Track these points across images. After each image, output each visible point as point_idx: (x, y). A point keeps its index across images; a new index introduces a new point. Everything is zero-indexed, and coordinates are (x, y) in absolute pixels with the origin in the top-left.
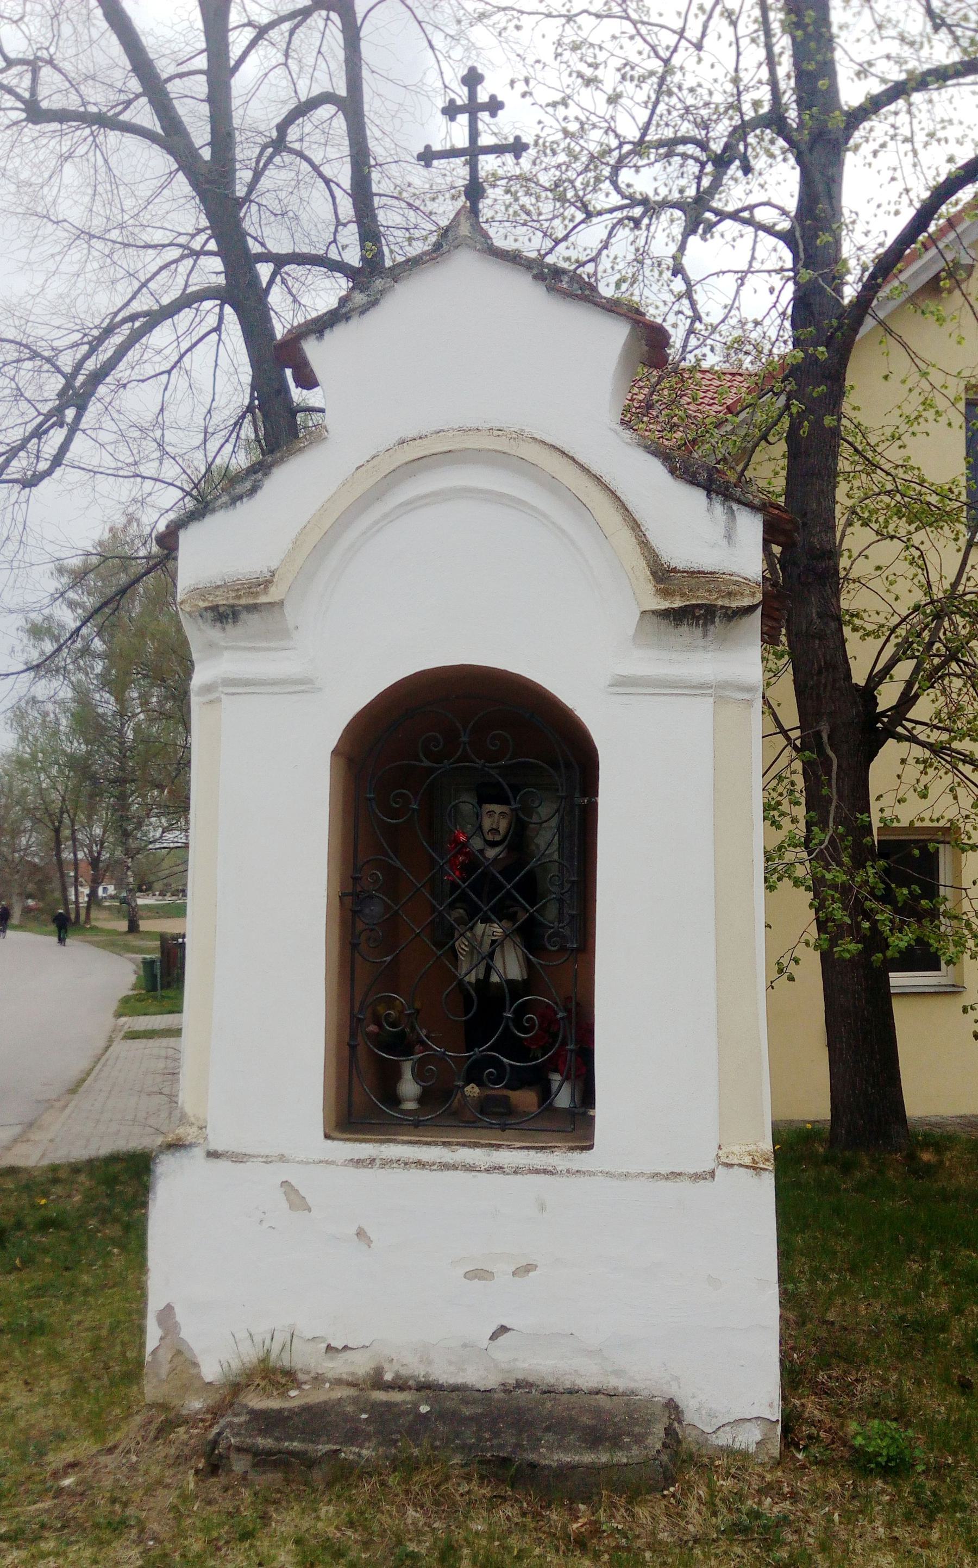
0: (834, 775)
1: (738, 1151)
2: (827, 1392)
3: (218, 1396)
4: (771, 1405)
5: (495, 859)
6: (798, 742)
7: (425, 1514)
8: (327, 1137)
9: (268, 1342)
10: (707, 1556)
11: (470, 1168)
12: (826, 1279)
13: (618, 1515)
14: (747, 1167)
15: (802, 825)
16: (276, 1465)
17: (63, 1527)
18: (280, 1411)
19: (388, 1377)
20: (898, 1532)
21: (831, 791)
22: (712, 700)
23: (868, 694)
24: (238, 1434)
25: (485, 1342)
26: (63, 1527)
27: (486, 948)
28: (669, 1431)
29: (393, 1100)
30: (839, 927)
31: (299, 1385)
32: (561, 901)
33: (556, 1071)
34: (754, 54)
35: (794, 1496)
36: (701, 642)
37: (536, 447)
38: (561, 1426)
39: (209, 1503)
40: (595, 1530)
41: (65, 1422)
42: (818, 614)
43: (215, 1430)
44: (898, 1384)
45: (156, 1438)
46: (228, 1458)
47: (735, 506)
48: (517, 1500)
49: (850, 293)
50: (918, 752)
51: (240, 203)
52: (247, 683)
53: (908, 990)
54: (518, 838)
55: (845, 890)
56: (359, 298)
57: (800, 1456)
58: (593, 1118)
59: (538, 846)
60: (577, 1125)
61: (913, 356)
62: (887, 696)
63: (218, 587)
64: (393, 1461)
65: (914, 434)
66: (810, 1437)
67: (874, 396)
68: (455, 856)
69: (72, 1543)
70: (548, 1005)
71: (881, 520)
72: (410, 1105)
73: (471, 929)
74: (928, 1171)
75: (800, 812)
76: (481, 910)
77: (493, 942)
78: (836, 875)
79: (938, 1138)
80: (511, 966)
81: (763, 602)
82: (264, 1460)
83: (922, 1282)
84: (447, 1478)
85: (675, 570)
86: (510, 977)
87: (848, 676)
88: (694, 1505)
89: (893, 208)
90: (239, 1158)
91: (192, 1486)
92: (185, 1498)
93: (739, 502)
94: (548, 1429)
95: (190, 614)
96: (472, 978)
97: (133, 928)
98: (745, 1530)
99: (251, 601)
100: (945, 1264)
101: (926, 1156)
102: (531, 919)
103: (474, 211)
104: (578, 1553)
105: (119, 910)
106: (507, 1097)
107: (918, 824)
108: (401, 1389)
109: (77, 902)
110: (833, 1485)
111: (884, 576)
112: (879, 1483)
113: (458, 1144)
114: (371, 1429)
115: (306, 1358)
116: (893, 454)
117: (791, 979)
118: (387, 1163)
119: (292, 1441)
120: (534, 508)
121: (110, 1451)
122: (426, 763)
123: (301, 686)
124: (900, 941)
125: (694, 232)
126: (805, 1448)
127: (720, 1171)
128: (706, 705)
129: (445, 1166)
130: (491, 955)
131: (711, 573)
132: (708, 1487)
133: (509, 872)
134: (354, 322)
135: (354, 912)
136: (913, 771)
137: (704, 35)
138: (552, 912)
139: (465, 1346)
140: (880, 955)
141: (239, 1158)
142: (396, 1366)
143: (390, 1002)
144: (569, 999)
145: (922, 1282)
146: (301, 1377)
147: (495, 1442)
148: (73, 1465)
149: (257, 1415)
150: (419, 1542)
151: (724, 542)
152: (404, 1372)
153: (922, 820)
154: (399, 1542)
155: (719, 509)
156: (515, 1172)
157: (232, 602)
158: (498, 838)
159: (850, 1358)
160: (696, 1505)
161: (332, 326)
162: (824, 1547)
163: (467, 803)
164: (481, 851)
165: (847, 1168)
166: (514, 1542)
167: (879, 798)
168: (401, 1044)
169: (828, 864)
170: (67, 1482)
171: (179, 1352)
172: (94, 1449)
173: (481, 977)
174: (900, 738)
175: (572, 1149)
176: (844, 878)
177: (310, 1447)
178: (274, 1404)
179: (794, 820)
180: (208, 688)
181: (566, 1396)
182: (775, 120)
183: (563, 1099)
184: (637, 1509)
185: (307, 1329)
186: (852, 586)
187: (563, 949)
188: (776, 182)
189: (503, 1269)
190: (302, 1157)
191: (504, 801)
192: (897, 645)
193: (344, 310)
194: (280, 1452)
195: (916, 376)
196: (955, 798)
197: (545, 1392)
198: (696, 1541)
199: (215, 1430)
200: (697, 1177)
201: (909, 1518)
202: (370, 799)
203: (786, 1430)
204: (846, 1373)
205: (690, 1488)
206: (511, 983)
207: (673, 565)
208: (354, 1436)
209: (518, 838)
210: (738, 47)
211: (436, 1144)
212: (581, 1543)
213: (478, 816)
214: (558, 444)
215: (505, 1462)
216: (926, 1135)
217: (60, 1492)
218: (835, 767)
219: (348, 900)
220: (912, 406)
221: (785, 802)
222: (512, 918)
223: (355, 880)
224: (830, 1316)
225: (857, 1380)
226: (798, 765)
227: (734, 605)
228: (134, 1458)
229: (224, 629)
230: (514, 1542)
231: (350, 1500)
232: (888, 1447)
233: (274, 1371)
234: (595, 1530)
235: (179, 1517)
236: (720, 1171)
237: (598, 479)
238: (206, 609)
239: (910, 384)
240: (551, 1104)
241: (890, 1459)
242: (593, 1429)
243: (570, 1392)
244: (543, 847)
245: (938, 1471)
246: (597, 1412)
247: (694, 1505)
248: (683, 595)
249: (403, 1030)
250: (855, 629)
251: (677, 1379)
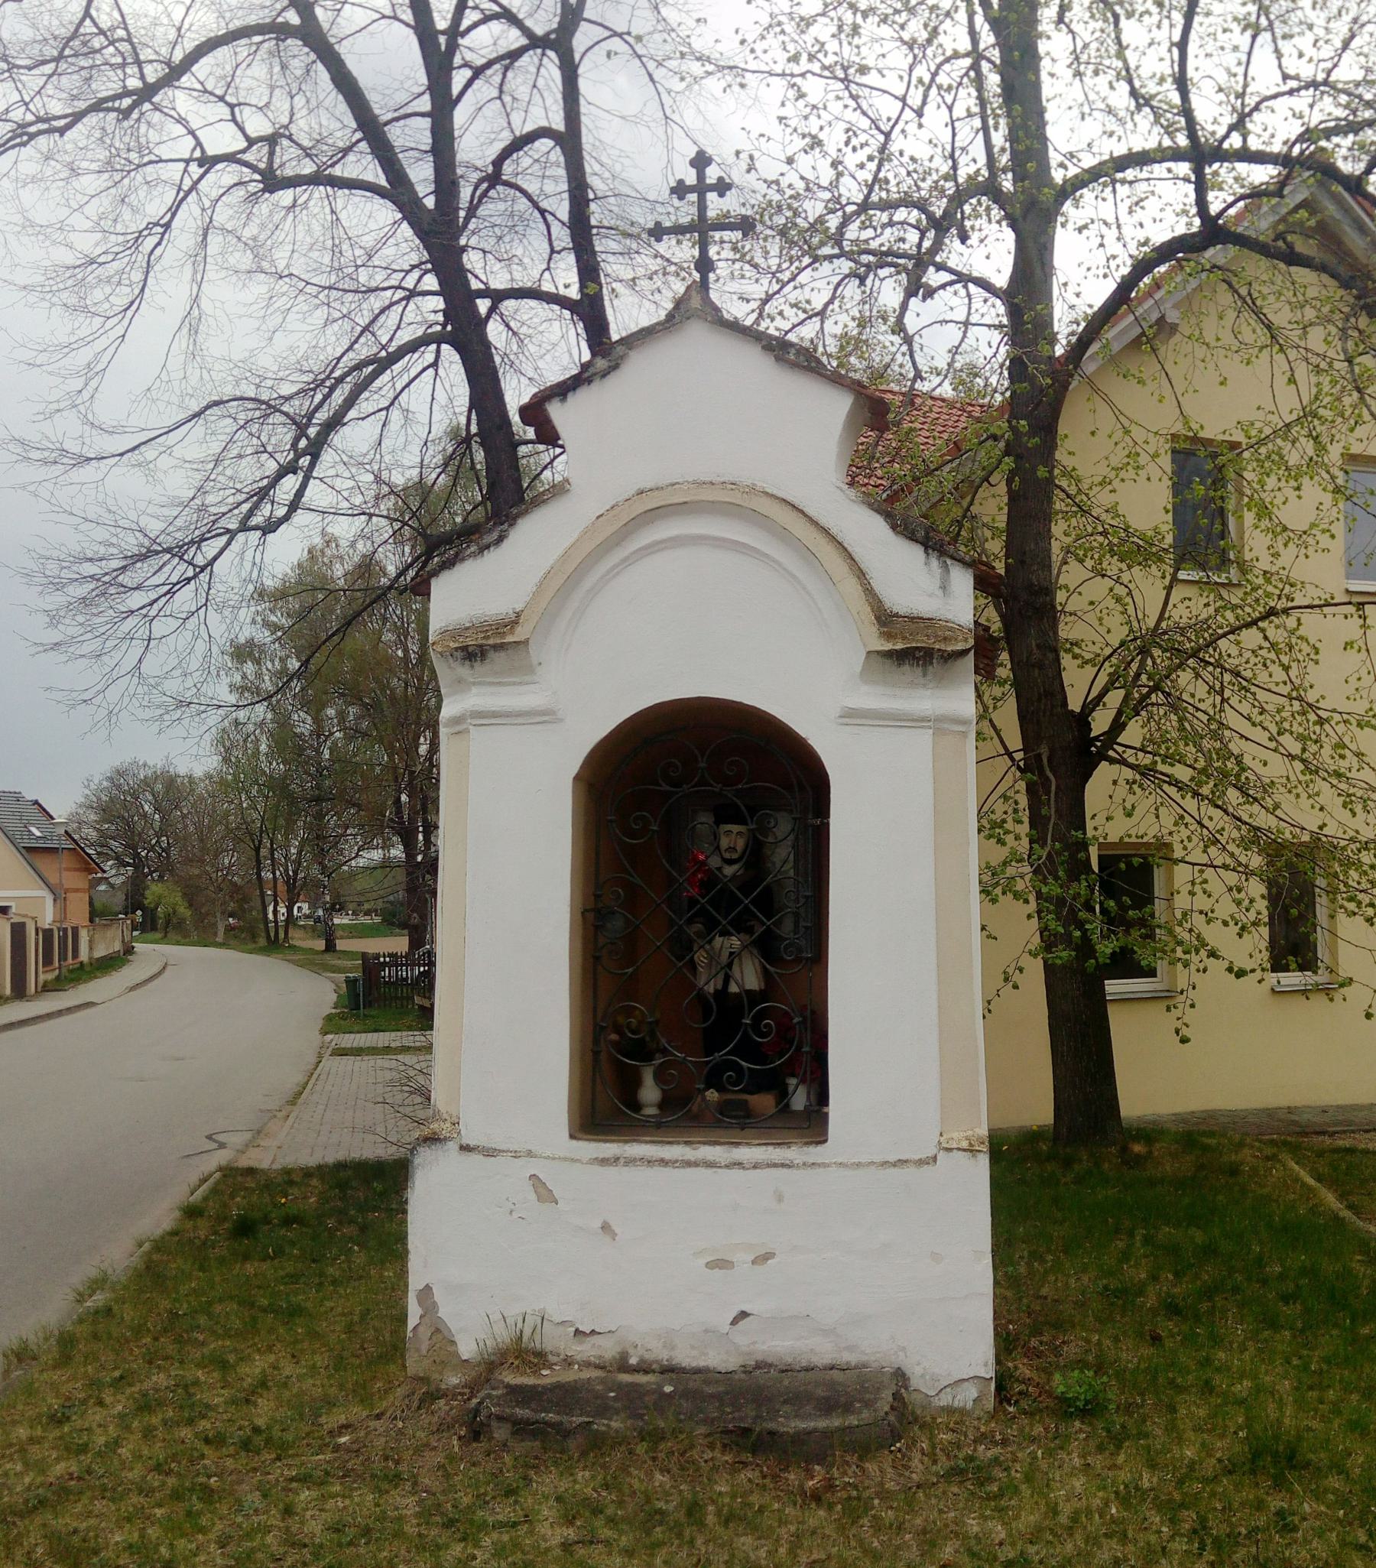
0: (1052, 795)
1: (958, 1137)
2: (1039, 1355)
3: (474, 1374)
4: (986, 1365)
5: (734, 876)
6: (1022, 764)
7: (673, 1477)
8: (572, 1137)
9: (520, 1325)
10: (928, 1496)
11: (711, 1165)
12: (1042, 1260)
13: (850, 1472)
14: (964, 1150)
15: (1025, 842)
16: (534, 1434)
17: (344, 1476)
18: (534, 1387)
19: (633, 1361)
20: (1090, 1460)
21: (1050, 811)
22: (931, 731)
23: (1082, 720)
24: (499, 1405)
25: (726, 1328)
26: (344, 1476)
27: (724, 958)
28: (896, 1396)
29: (637, 1106)
30: (1055, 935)
31: (550, 1366)
32: (796, 915)
33: (793, 1075)
34: (967, 131)
35: (1005, 1442)
36: (922, 680)
37: (767, 501)
38: (797, 1399)
39: (474, 1465)
40: (830, 1486)
41: (333, 1391)
42: (1038, 646)
43: (475, 1401)
44: (1099, 1343)
45: (419, 1408)
46: (489, 1426)
47: (949, 562)
48: (757, 1465)
50: (1128, 773)
51: (488, 288)
52: (495, 715)
53: (1132, 996)
54: (755, 855)
55: (1060, 902)
56: (601, 364)
57: (1011, 1409)
58: (827, 1114)
59: (774, 864)
60: (812, 1123)
61: (1118, 413)
62: (1100, 723)
63: (467, 629)
64: (640, 1433)
65: (1123, 480)
66: (1020, 1393)
67: (1084, 445)
68: (694, 874)
69: (356, 1489)
70: (786, 1013)
71: (1096, 556)
72: (651, 1111)
73: (710, 942)
74: (1138, 1161)
75: (1024, 829)
76: (720, 923)
77: (731, 954)
78: (1053, 889)
79: (1149, 1133)
80: (749, 977)
81: (976, 646)
82: (522, 1429)
83: (1125, 1256)
84: (692, 1447)
85: (897, 615)
86: (747, 987)
87: (1065, 703)
88: (916, 1456)
89: (1101, 272)
90: (490, 1153)
91: (456, 1449)
92: (451, 1458)
93: (953, 558)
94: (785, 1402)
95: (441, 653)
96: (710, 988)
97: (330, 947)
98: (962, 1472)
100: (1147, 1240)
101: (1138, 1148)
102: (768, 930)
103: (704, 285)
104: (813, 1505)
105: (313, 929)
106: (746, 1101)
107: (1126, 840)
108: (646, 1372)
109: (276, 921)
110: (1038, 1429)
111: (1098, 610)
112: (1077, 1424)
113: (699, 1142)
114: (618, 1405)
115: (556, 1341)
116: (1102, 498)
117: (1016, 987)
118: (630, 1162)
119: (545, 1414)
120: (766, 555)
121: (378, 1417)
123: (544, 716)
124: (1105, 948)
125: (915, 294)
126: (1017, 1402)
127: (941, 1155)
128: (924, 739)
129: (689, 1164)
130: (730, 965)
132: (930, 1439)
133: (746, 887)
134: (596, 386)
135: (597, 928)
136: (1122, 790)
137: (924, 103)
138: (788, 926)
139: (706, 1331)
140: (1093, 961)
141: (490, 1153)
142: (640, 1351)
143: (629, 1011)
144: (805, 1007)
145: (1125, 1256)
146: (552, 1359)
147: (736, 1415)
148: (346, 1427)
149: (513, 1390)
150: (667, 1502)
151: (940, 593)
152: (647, 1356)
153: (1130, 836)
154: (648, 1501)
155: (935, 563)
156: (755, 1167)
157: (480, 642)
158: (735, 856)
159: (1059, 1325)
160: (919, 1455)
161: (574, 389)
162: (1028, 1479)
163: (704, 820)
164: (719, 869)
165: (1067, 1163)
166: (755, 1499)
167: (1093, 817)
168: (642, 1052)
169: (1045, 878)
170: (343, 1440)
171: (438, 1330)
172: (365, 1414)
173: (719, 987)
174: (1112, 761)
175: (807, 1144)
176: (1059, 890)
177: (565, 1419)
178: (530, 1381)
179: (1017, 838)
180: (457, 720)
181: (802, 1374)
182: (990, 189)
183: (799, 1100)
184: (867, 1465)
185: (557, 1312)
186: (1069, 619)
187: (798, 960)
188: (991, 250)
189: (742, 1258)
190: (548, 1153)
191: (741, 821)
192: (1110, 674)
193: (586, 375)
194: (537, 1422)
195: (1120, 433)
196: (1157, 817)
197: (783, 1371)
198: (918, 1487)
199: (475, 1401)
200: (921, 1163)
201: (1100, 1449)
202: (611, 821)
203: (999, 1388)
204: (1055, 1338)
205: (914, 1442)
206: (749, 992)
207: (895, 611)
208: (604, 1410)
209: (755, 855)
210: (953, 129)
211: (678, 1143)
212: (816, 1497)
213: (716, 837)
214: (789, 498)
215: (746, 1432)
216: (1138, 1129)
217: (337, 1448)
218: (1053, 788)
219: (591, 916)
220: (1118, 458)
221: (1010, 820)
222: (749, 931)
223: (597, 897)
224: (1044, 1291)
225: (1064, 1342)
226: (1022, 785)
227: (949, 649)
228: (400, 1424)
229: (472, 667)
230: (755, 1499)
231: (604, 1467)
232: (1086, 1391)
233: (527, 1351)
234: (830, 1486)
235: (447, 1476)
236: (941, 1155)
237: (825, 531)
238: (456, 649)
239: (1115, 438)
240: (787, 1105)
241: (1087, 1402)
242: (827, 1399)
243: (807, 1369)
244: (778, 866)
245: (1128, 1409)
246: (832, 1385)
247: (916, 1456)
248: (904, 638)
249: (643, 1040)
250: (1075, 657)
251: (904, 1349)
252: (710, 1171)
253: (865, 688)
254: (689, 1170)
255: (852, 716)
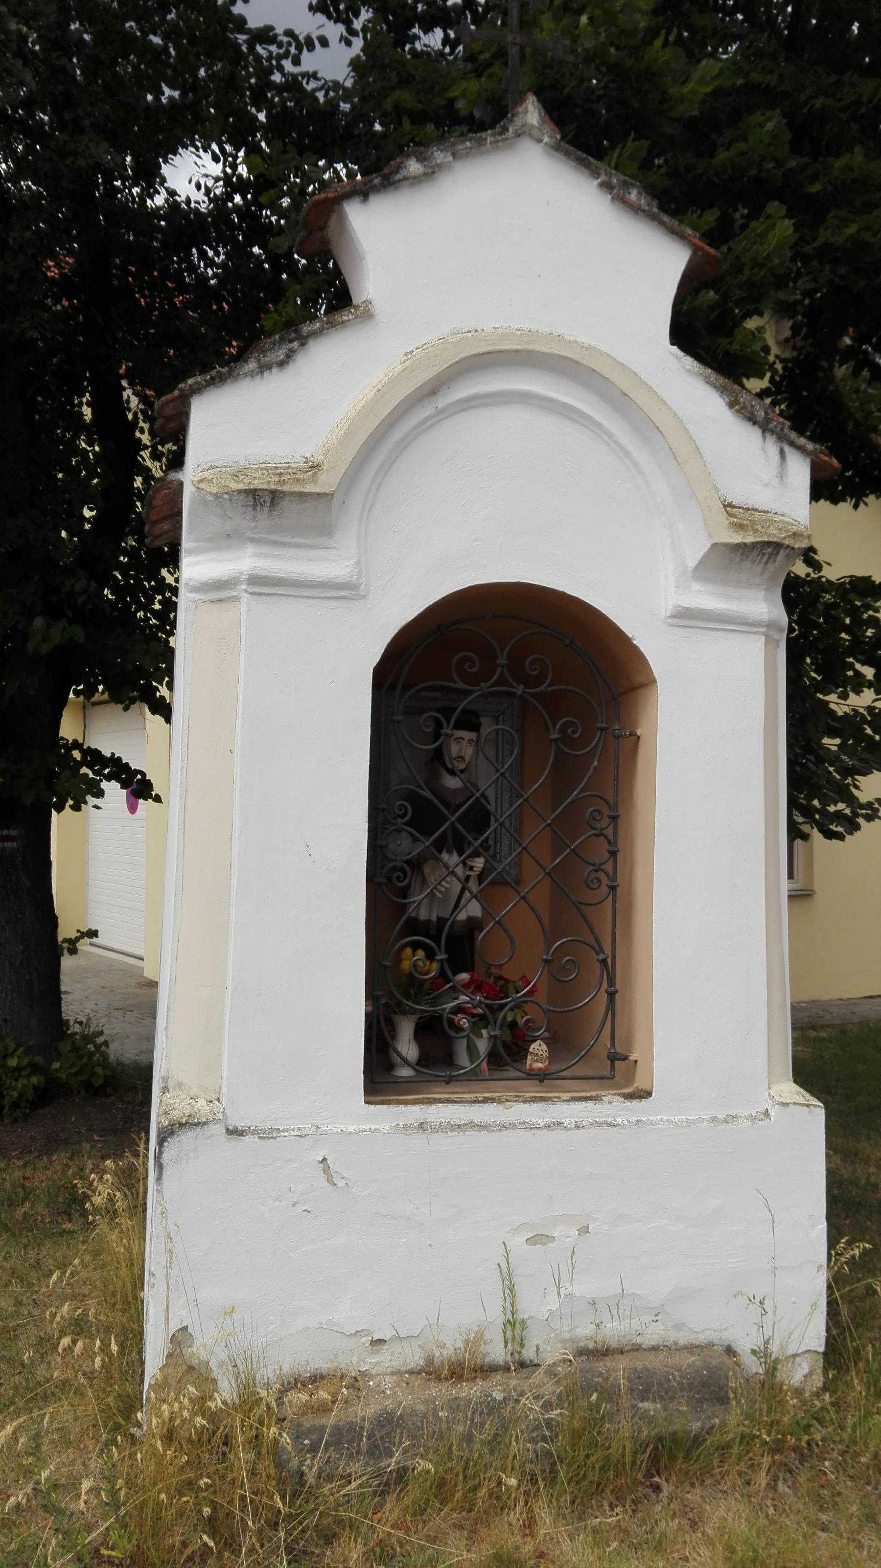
47: (787, 448)
49: (396, 178)
99: (297, 488)
122: (460, 685)
123: (345, 591)
131: (764, 512)
141: (267, 1134)
151: (776, 482)
157: (273, 487)
180: (218, 589)
252: (530, 1133)
253: (696, 586)
254: (505, 1133)
255: (686, 617)
